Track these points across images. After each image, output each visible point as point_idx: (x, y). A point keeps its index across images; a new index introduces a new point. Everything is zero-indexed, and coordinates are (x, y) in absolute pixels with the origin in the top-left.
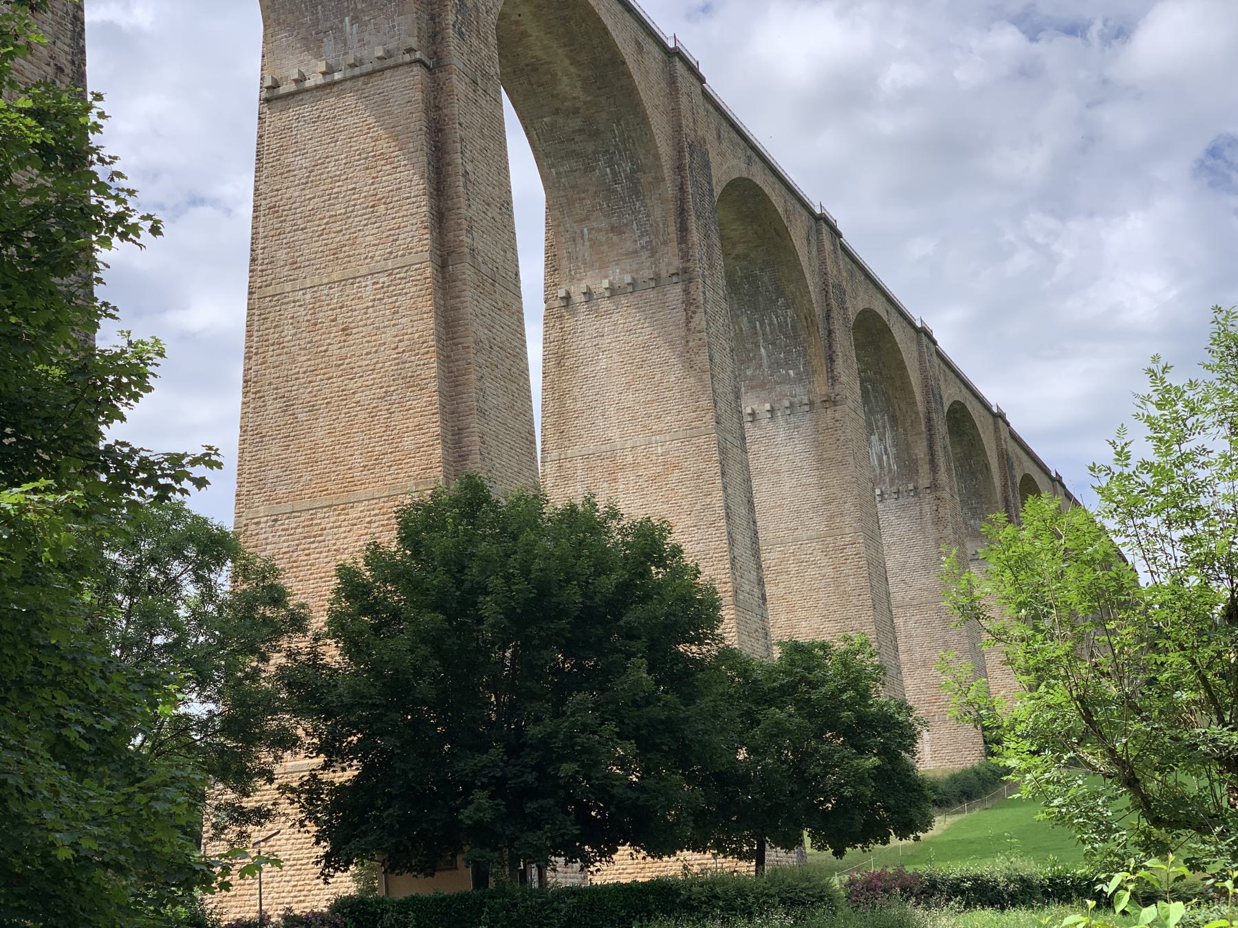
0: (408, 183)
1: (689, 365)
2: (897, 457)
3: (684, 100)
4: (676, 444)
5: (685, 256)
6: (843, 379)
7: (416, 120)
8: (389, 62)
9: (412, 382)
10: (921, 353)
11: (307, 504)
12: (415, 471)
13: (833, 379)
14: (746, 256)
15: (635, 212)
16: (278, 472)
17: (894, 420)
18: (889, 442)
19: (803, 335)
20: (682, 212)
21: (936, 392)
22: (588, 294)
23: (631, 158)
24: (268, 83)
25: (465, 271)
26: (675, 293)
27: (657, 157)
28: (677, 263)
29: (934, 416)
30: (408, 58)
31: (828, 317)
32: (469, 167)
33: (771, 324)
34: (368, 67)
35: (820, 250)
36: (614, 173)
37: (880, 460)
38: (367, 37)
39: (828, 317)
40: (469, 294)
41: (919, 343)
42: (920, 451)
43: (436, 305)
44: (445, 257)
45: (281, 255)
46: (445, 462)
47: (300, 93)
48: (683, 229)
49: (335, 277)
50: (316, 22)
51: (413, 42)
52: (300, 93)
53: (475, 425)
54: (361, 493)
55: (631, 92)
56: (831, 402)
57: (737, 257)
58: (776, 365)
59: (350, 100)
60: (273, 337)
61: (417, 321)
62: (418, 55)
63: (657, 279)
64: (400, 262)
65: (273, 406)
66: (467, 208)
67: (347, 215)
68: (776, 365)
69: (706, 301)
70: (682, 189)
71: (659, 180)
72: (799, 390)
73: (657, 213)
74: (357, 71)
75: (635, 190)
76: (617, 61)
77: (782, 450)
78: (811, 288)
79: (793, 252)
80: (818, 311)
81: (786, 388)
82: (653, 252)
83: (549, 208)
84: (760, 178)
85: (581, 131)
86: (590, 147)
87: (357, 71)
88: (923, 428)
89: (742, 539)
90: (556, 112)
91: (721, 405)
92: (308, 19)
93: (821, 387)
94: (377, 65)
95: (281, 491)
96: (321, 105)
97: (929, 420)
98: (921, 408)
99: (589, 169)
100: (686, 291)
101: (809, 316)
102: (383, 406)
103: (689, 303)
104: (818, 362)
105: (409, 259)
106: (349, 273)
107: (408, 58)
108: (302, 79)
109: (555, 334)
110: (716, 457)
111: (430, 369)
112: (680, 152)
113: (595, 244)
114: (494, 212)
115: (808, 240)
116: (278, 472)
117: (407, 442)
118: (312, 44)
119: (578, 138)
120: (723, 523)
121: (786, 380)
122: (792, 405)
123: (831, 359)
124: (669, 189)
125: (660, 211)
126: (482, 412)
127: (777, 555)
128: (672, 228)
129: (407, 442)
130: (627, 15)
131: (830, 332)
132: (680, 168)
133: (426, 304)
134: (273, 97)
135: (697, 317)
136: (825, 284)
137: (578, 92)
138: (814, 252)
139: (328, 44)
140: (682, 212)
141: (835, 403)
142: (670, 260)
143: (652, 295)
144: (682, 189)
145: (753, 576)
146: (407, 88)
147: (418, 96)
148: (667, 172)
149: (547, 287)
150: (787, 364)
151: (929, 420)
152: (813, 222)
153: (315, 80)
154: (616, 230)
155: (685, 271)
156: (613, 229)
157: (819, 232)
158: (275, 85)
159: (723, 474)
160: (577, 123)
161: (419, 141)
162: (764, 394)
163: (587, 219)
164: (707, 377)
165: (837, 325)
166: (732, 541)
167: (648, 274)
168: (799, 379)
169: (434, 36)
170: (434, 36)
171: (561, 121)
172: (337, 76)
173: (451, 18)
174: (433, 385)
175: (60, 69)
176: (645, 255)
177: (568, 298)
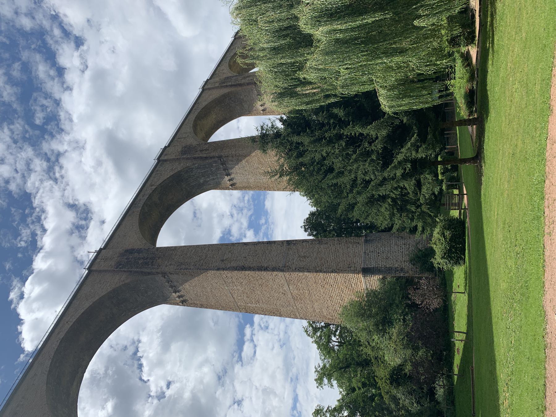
9: (284, 320)
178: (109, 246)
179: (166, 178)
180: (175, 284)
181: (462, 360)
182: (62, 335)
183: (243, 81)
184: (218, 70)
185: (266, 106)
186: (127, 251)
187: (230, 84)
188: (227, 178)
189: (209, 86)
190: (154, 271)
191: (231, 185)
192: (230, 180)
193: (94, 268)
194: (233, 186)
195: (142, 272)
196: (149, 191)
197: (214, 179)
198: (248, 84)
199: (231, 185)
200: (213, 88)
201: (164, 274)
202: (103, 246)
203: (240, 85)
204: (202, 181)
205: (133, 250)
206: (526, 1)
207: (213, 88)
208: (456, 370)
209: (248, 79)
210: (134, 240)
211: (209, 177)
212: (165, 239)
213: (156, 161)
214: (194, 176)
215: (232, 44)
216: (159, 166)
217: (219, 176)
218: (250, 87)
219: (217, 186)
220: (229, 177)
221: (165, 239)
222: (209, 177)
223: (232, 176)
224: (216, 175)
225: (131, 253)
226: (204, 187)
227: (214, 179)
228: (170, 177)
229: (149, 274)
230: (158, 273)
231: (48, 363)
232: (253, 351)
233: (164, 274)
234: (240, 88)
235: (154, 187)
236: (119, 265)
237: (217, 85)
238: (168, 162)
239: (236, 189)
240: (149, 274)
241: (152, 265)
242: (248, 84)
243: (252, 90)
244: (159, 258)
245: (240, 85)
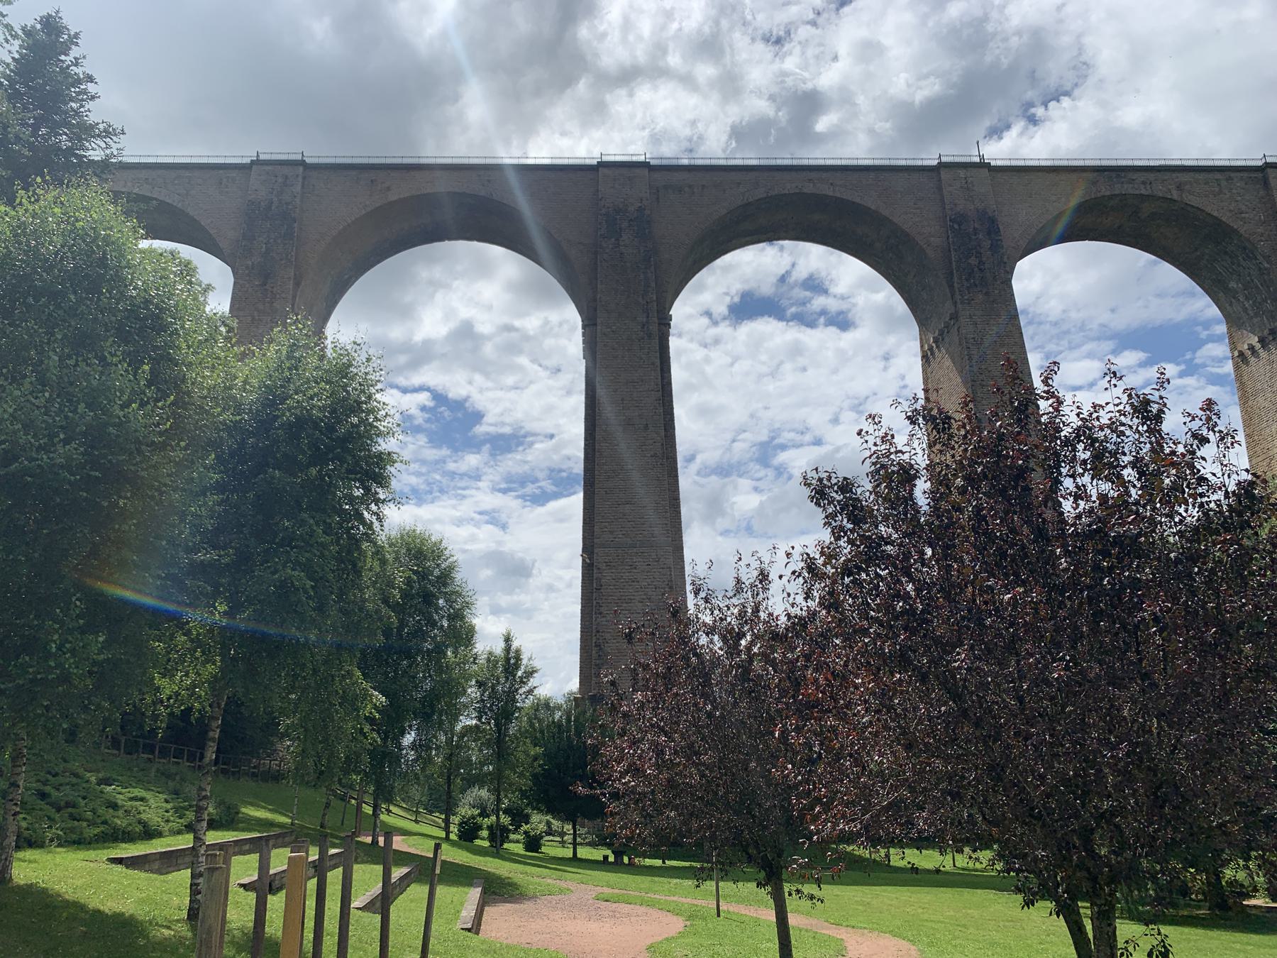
178: (999, 175)
179: (1208, 210)
180: (947, 339)
181: (860, 860)
182: (809, 189)
186: (993, 221)
188: (1254, 340)
190: (958, 297)
191: (1241, 354)
192: (1252, 348)
193: (944, 174)
194: (1241, 359)
195: (952, 273)
196: (1159, 189)
197: (1245, 310)
199: (1241, 354)
201: (955, 317)
202: (999, 163)
204: (1232, 285)
205: (998, 232)
208: (1091, 936)
211: (1247, 298)
212: (341, 869)
213: (1260, 163)
214: (1239, 265)
216: (1246, 175)
217: (1255, 320)
219: (1233, 321)
221: (341, 869)
222: (1247, 298)
223: (1263, 354)
224: (1256, 315)
225: (989, 233)
226: (1221, 294)
227: (1245, 310)
228: (1216, 218)
229: (951, 286)
230: (955, 303)
231: (760, 193)
232: (1078, 382)
233: (955, 317)
235: (1175, 195)
236: (960, 219)
238: (1262, 193)
239: (1237, 367)
240: (951, 286)
241: (968, 288)
244: (987, 294)
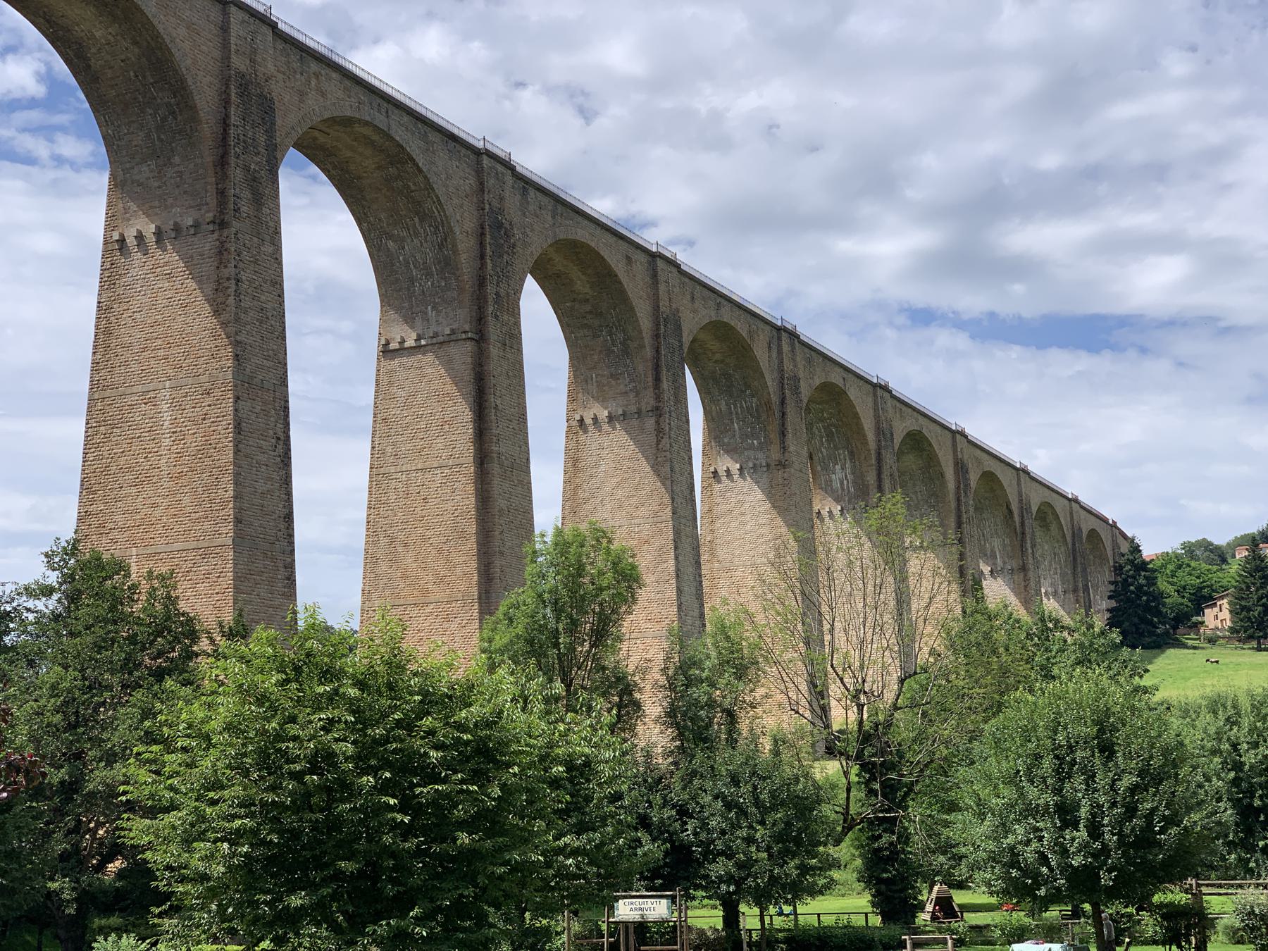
0: (463, 413)
1: (658, 473)
2: (854, 482)
3: (662, 287)
4: (647, 526)
5: (658, 398)
6: (792, 449)
7: (468, 375)
8: (453, 337)
9: (462, 536)
10: (876, 403)
11: (401, 601)
12: (462, 588)
13: (784, 449)
14: (722, 361)
15: (627, 366)
16: (385, 581)
17: (852, 454)
18: (848, 471)
19: (764, 417)
20: (657, 368)
21: (887, 432)
22: (595, 419)
23: (623, 330)
24: (383, 342)
25: (495, 468)
26: (650, 423)
27: (640, 332)
28: (652, 402)
29: (883, 452)
30: (464, 336)
31: (783, 402)
32: (498, 402)
33: (742, 407)
34: (441, 339)
35: (780, 352)
36: (612, 340)
37: (842, 483)
38: (441, 319)
39: (783, 402)
40: (496, 481)
41: (875, 395)
42: (871, 478)
43: (476, 489)
44: (482, 458)
45: (389, 449)
46: (480, 584)
47: (402, 350)
48: (657, 379)
49: (420, 466)
50: (411, 308)
51: (467, 327)
52: (402, 350)
53: (498, 562)
54: (432, 598)
55: (622, 292)
56: (782, 465)
57: (716, 362)
58: (745, 436)
59: (430, 357)
60: (384, 499)
61: (467, 501)
62: (470, 335)
63: (639, 412)
64: (457, 461)
65: (383, 542)
66: (498, 428)
67: (427, 429)
68: (745, 436)
69: (670, 429)
70: (658, 351)
71: (642, 346)
72: (760, 455)
73: (641, 368)
74: (434, 341)
75: (626, 352)
76: (611, 275)
77: (747, 498)
78: (769, 384)
79: (755, 359)
80: (775, 399)
81: (751, 453)
82: (637, 395)
83: (571, 359)
84: (727, 316)
85: (590, 312)
86: (597, 323)
87: (434, 341)
88: (873, 462)
89: (689, 589)
90: (574, 300)
91: (679, 500)
92: (406, 305)
93: (775, 455)
94: (446, 338)
95: (387, 593)
96: (413, 358)
97: (879, 454)
98: (872, 445)
99: (596, 336)
100: (658, 423)
101: (768, 403)
102: (445, 547)
103: (659, 431)
104: (774, 436)
105: (462, 460)
106: (427, 465)
107: (464, 336)
108: (403, 341)
109: (573, 444)
110: (671, 537)
111: (472, 529)
112: (657, 325)
113: (599, 384)
114: (514, 424)
115: (770, 348)
116: (385, 581)
117: (459, 571)
118: (409, 320)
119: (589, 316)
120: (674, 581)
121: (751, 447)
122: (755, 465)
123: (783, 434)
124: (649, 352)
125: (643, 367)
126: (502, 553)
127: (739, 574)
128: (650, 379)
129: (459, 571)
130: (620, 242)
131: (784, 414)
132: (657, 336)
133: (471, 489)
134: (386, 352)
135: (664, 441)
136: (782, 378)
137: (587, 290)
138: (774, 355)
139: (418, 321)
140: (657, 368)
141: (784, 467)
142: (648, 400)
143: (635, 423)
144: (658, 351)
145: (696, 613)
146: (463, 353)
147: (469, 360)
148: (648, 340)
149: (568, 412)
150: (753, 436)
151: (879, 454)
152: (775, 332)
153: (410, 343)
154: (614, 376)
155: (657, 408)
156: (612, 376)
157: (779, 339)
158: (387, 343)
159: (676, 548)
160: (588, 308)
161: (471, 388)
162: (736, 456)
163: (594, 368)
164: (668, 483)
165: (790, 409)
166: (679, 591)
167: (633, 408)
168: (760, 448)
169: (480, 320)
170: (480, 320)
171: (577, 306)
172: (423, 342)
173: (491, 308)
174: (474, 538)
175: (278, 439)
176: (632, 395)
177: (581, 421)
183: (236, 174)
184: (325, 71)
185: (137, 257)
187: (234, 119)
188: (149, 229)
189: (236, 29)
192: (140, 237)
198: (222, 193)
200: (225, 45)
203: (222, 163)
206: (1265, 888)
207: (225, 45)
209: (246, 194)
210: (296, 107)
215: (452, 137)
218: (212, 200)
220: (735, 473)
223: (606, 427)
234: (209, 158)
237: (239, 63)
242: (222, 193)
243: (199, 207)
245: (222, 163)
